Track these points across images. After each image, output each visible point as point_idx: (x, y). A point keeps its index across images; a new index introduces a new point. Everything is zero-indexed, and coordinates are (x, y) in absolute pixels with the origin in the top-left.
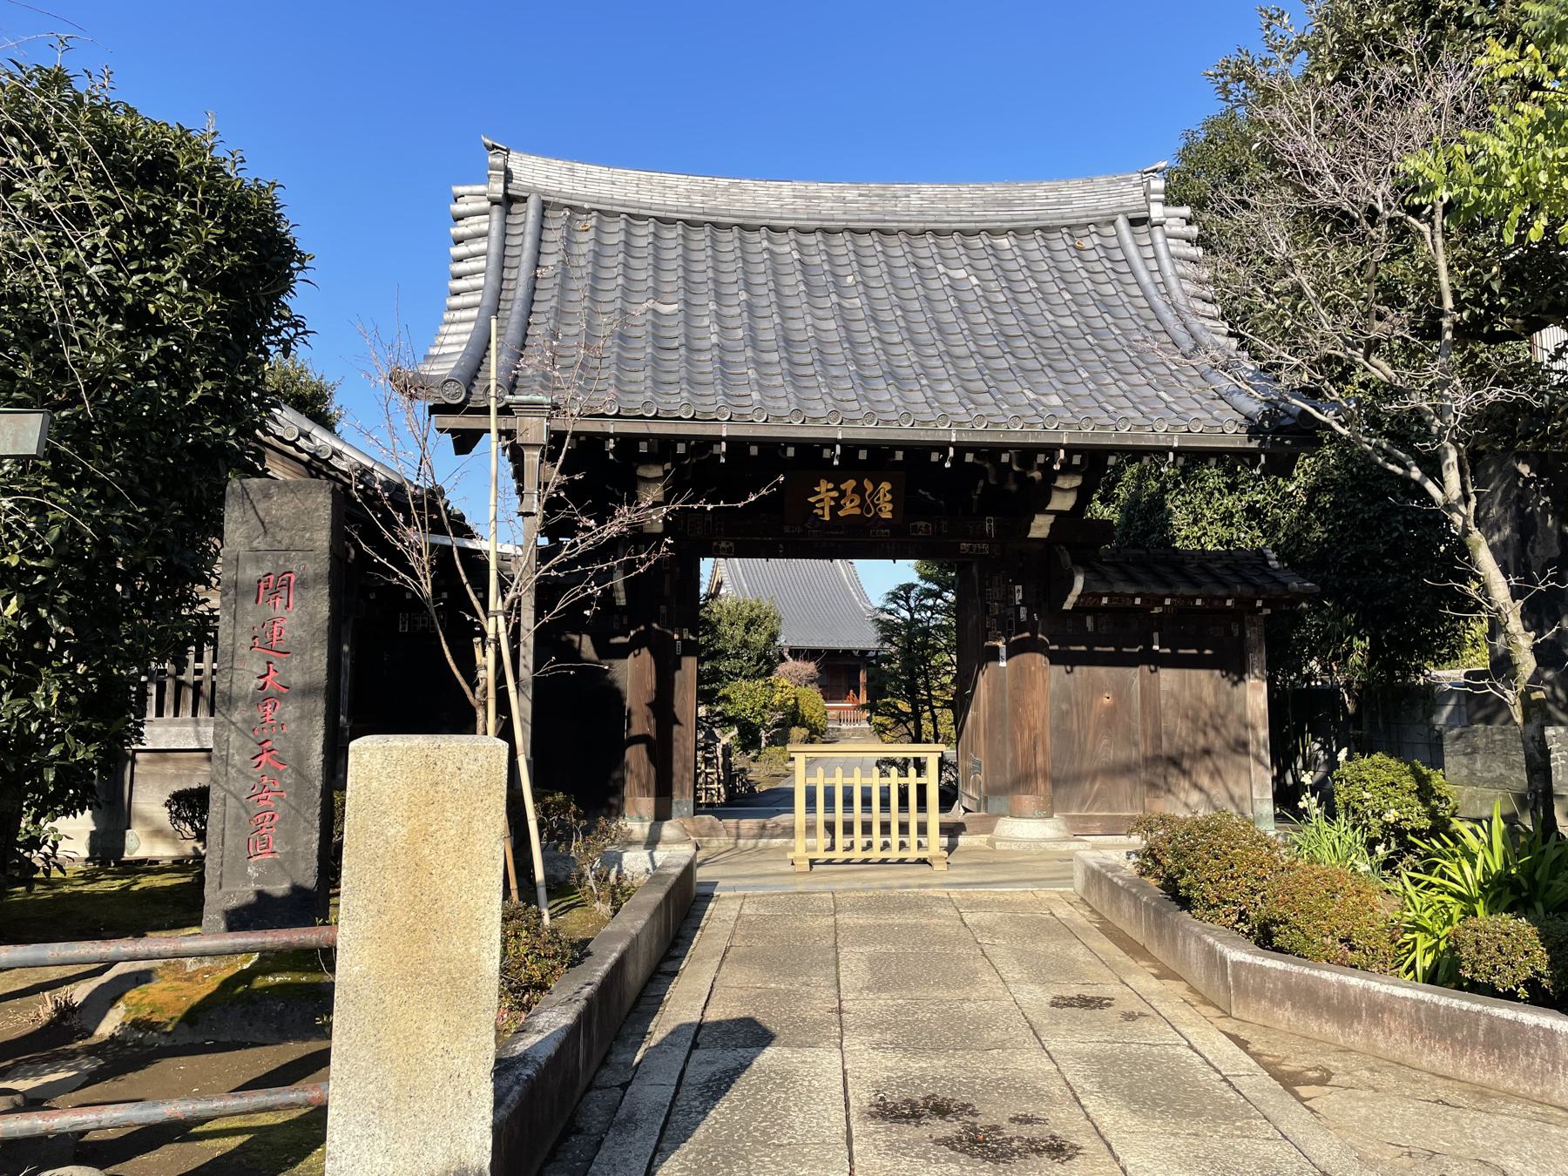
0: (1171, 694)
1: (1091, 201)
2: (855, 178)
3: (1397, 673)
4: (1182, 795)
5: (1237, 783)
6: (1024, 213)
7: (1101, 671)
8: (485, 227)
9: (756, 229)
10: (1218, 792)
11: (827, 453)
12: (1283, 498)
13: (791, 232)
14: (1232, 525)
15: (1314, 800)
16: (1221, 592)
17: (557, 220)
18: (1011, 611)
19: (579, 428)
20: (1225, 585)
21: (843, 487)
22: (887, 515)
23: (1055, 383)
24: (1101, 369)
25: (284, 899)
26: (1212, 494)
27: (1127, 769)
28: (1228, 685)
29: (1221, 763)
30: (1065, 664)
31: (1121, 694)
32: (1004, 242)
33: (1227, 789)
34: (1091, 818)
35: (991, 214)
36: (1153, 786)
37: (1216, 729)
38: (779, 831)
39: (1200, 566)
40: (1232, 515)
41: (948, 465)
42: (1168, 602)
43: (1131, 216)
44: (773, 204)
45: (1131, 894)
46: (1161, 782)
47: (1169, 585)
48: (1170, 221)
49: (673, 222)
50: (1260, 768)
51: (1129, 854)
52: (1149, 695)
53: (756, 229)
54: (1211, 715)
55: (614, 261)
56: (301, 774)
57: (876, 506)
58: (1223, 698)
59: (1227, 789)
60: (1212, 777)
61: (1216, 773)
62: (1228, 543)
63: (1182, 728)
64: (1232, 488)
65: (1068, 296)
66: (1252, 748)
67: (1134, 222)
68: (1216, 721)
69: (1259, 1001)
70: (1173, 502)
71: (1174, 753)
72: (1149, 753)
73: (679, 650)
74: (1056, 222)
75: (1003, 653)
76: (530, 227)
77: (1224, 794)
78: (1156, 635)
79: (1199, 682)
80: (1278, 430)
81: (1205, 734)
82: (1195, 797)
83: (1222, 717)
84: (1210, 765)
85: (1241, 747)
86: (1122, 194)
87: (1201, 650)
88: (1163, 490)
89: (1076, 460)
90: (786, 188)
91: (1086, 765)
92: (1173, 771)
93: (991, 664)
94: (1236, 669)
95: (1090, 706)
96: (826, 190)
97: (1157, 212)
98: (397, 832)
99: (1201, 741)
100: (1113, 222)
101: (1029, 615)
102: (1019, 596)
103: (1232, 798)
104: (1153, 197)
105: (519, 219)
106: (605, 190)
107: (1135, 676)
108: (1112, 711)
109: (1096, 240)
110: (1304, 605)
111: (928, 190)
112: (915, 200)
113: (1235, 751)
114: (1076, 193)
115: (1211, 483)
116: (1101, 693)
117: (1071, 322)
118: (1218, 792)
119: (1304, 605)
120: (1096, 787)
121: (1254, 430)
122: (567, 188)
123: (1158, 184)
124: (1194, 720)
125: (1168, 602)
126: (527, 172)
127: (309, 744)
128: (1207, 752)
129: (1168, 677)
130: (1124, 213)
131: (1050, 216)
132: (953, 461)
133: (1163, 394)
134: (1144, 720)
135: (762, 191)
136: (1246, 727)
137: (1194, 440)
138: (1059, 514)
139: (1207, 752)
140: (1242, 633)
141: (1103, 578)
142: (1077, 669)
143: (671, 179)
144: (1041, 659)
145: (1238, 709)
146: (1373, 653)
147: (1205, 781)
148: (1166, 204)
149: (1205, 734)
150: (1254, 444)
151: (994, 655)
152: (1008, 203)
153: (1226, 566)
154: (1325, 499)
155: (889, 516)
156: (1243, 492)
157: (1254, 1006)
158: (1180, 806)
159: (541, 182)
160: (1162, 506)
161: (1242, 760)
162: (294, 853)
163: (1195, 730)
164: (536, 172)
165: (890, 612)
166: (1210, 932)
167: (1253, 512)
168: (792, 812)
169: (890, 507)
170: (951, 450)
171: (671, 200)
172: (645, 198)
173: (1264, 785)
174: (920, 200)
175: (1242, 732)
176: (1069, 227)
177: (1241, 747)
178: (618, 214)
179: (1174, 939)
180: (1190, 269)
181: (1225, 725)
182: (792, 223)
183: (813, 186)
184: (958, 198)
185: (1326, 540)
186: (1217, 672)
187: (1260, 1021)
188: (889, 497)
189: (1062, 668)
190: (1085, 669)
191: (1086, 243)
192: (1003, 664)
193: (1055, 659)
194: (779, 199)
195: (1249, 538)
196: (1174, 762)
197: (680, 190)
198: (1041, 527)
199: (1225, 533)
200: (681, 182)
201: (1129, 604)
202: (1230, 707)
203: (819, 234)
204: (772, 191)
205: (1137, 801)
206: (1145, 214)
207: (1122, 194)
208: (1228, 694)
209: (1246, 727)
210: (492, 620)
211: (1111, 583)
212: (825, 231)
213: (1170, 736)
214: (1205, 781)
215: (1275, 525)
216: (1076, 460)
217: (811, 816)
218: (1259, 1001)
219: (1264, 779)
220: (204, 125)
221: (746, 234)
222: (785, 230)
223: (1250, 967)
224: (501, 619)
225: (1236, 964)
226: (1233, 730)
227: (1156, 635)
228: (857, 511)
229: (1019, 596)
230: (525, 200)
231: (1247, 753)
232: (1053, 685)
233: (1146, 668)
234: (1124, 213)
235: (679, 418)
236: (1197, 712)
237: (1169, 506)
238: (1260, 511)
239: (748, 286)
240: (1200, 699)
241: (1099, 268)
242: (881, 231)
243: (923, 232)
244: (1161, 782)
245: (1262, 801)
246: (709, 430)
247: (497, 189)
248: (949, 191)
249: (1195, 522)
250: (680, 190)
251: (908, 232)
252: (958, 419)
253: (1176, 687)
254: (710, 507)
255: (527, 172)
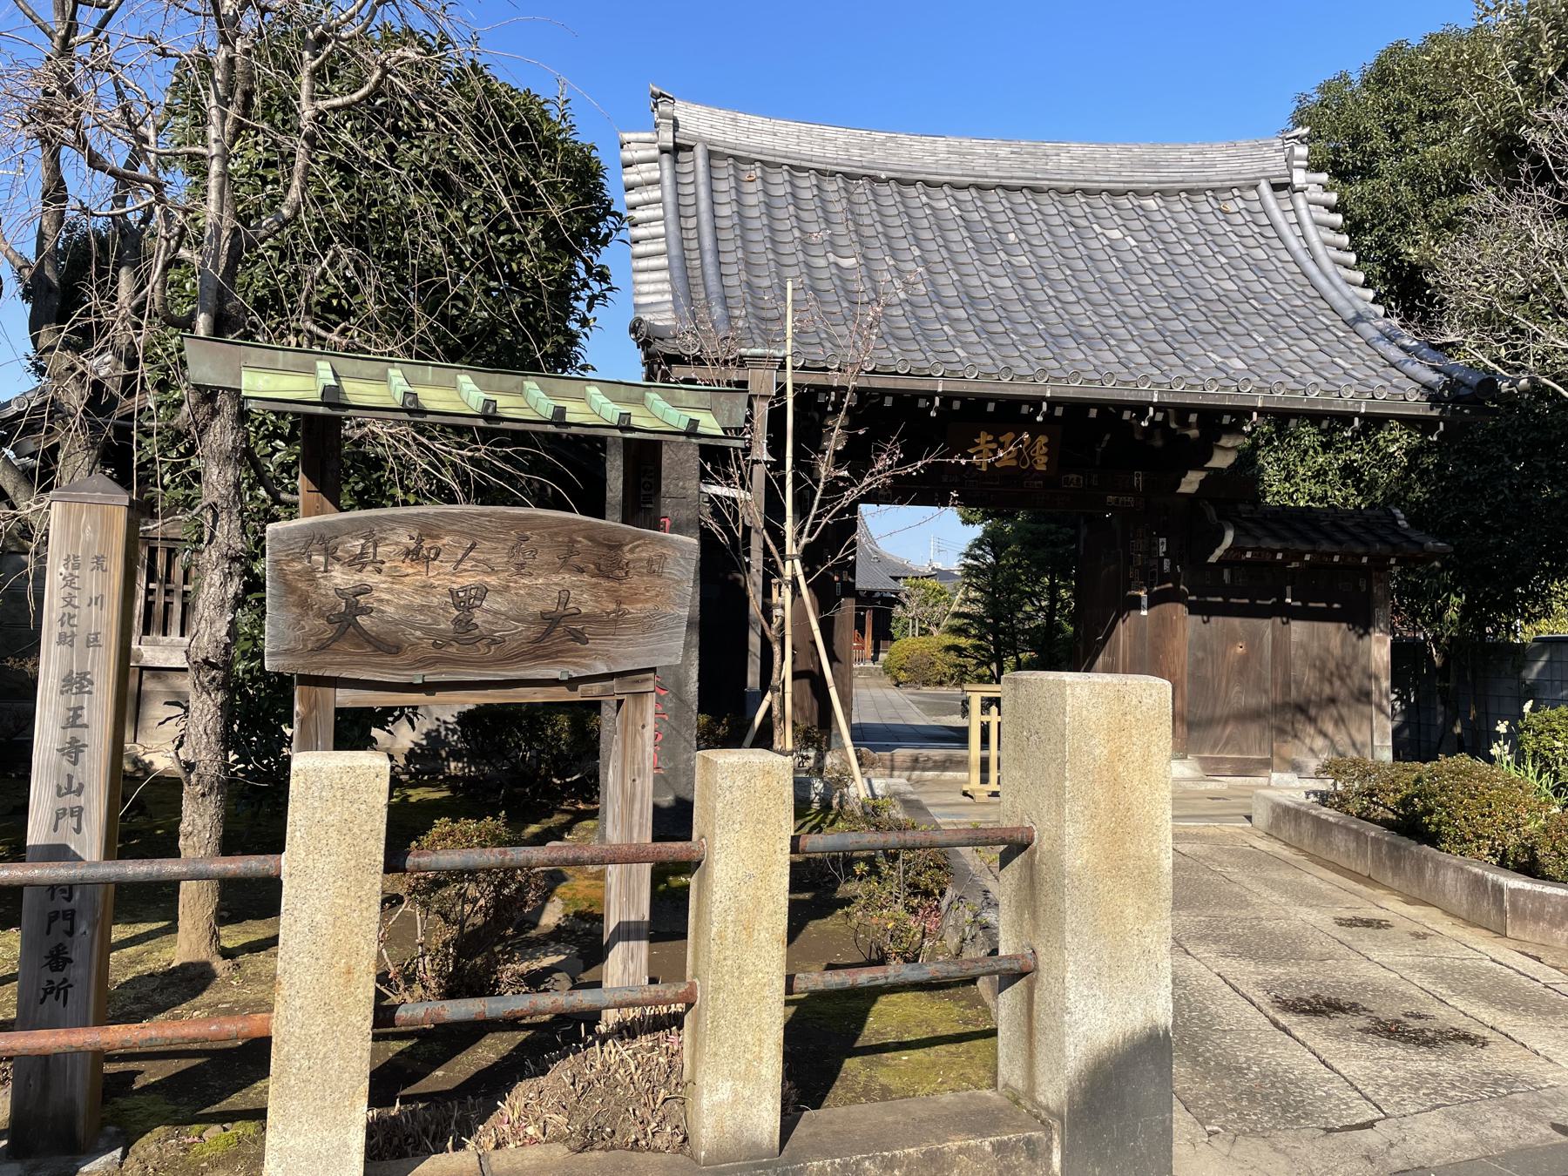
0: (1301, 645)
1: (1234, 164)
2: (1007, 139)
3: (1489, 630)
4: (1308, 741)
5: (1359, 730)
6: (1169, 175)
7: (1236, 622)
8: (656, 175)
9: (913, 183)
10: (1341, 739)
11: (821, 399)
12: (1382, 459)
13: (919, 185)
14: (1324, 482)
15: (1507, 748)
16: (1360, 550)
17: (725, 169)
18: (1155, 562)
19: (864, 383)
20: (1365, 543)
21: (1001, 439)
22: (1041, 467)
23: (1235, 347)
24: (1272, 333)
25: (670, 809)
26: (1306, 452)
27: (1256, 715)
28: (1354, 639)
29: (1345, 711)
30: (1281, 616)
31: (1253, 642)
32: (1150, 203)
33: (1350, 736)
34: (1222, 760)
35: (1138, 176)
36: (1281, 731)
37: (1342, 679)
38: (930, 764)
39: (1333, 524)
40: (1326, 473)
41: (1039, 419)
42: (1307, 558)
43: (1274, 181)
44: (929, 160)
45: (1349, 830)
46: (1289, 728)
47: (1313, 542)
48: (1311, 187)
49: (833, 174)
50: (1382, 717)
51: (1308, 794)
52: (1279, 646)
53: (913, 183)
54: (1337, 665)
55: (785, 212)
56: (681, 701)
57: (1031, 458)
58: (1350, 650)
59: (1350, 736)
60: (1336, 724)
61: (1340, 721)
62: (1323, 498)
63: (1309, 677)
64: (1326, 447)
65: (1223, 260)
66: (1375, 697)
67: (1276, 187)
68: (1342, 671)
69: (1537, 923)
70: (1266, 458)
71: (1301, 700)
72: (1279, 700)
73: (839, 592)
74: (1202, 185)
75: (1145, 602)
76: (702, 177)
77: (1348, 741)
78: (1289, 589)
79: (1327, 634)
80: (1456, 400)
81: (1331, 683)
82: (1319, 743)
83: (1348, 668)
84: (1335, 713)
85: (1364, 696)
86: (1264, 159)
87: (1330, 604)
88: (1255, 447)
89: (1059, 412)
90: (941, 144)
91: (1218, 712)
92: (1299, 717)
93: (1133, 613)
94: (1361, 622)
95: (1224, 655)
96: (979, 147)
97: (1299, 177)
98: (1101, 752)
99: (1327, 690)
100: (1256, 187)
101: (1172, 567)
102: (1163, 549)
103: (1354, 744)
104: (1296, 163)
105: (688, 168)
106: (767, 141)
107: (1267, 627)
108: (1245, 659)
109: (1241, 204)
110: (1437, 564)
111: (1077, 149)
112: (1065, 159)
113: (1358, 700)
114: (1219, 156)
115: (1306, 441)
116: (1235, 642)
117: (1230, 285)
118: (1341, 739)
119: (1437, 564)
120: (1228, 731)
121: (1434, 398)
122: (730, 139)
123: (1302, 151)
124: (1322, 671)
125: (1307, 558)
126: (692, 121)
127: (687, 672)
128: (1332, 700)
129: (1298, 629)
130: (1267, 178)
131: (1195, 179)
132: (1045, 416)
133: (1338, 360)
134: (1274, 668)
135: (918, 146)
136: (1370, 677)
137: (1381, 406)
138: (1199, 467)
139: (1332, 700)
140: (1370, 588)
141: (1248, 533)
142: (1213, 619)
143: (830, 132)
144: (1181, 609)
145: (1362, 661)
146: (1465, 611)
147: (1329, 728)
148: (1307, 169)
149: (1331, 683)
150: (1435, 413)
151: (1136, 604)
152: (1154, 165)
153: (1358, 525)
154: (1429, 461)
155: (1044, 468)
156: (1340, 451)
157: (1531, 927)
158: (1305, 750)
159: (706, 131)
160: (1254, 462)
161: (1366, 709)
162: (675, 769)
163: (1322, 679)
164: (700, 121)
165: (975, 558)
166: (1470, 863)
167: (1348, 470)
168: (966, 748)
169: (1045, 459)
170: (1045, 405)
171: (830, 152)
172: (805, 150)
173: (1384, 733)
174: (1069, 159)
175: (1366, 682)
176: (1213, 190)
177: (1364, 696)
178: (780, 166)
179: (1420, 871)
180: (1330, 236)
181: (1349, 676)
182: (947, 178)
183: (966, 142)
184: (1107, 158)
185: (1426, 501)
186: (1344, 625)
187: (1538, 940)
188: (1045, 449)
189: (1199, 618)
190: (1221, 619)
191: (1231, 207)
192: (1144, 613)
193: (1194, 609)
194: (934, 154)
195: (1341, 495)
196: (1301, 709)
197: (839, 142)
198: (1191, 482)
199: (1318, 490)
200: (839, 135)
201: (1268, 557)
202: (1355, 658)
203: (973, 190)
204: (928, 146)
205: (1265, 746)
206: (1287, 180)
207: (1264, 159)
208: (1354, 646)
209: (1370, 677)
210: (788, 563)
211: (1258, 539)
212: (979, 187)
213: (1299, 684)
214: (1329, 728)
215: (1373, 483)
216: (1059, 412)
217: (985, 753)
218: (1537, 923)
219: (1385, 727)
220: (543, 92)
221: (904, 189)
222: (940, 185)
223: (1527, 894)
224: (797, 562)
225: (1514, 892)
226: (1357, 680)
227: (1289, 589)
228: (1014, 463)
229: (1163, 549)
230: (691, 148)
231: (1370, 703)
232: (1189, 632)
233: (1278, 620)
234: (1267, 178)
235: (896, 373)
236: (1323, 662)
237: (1261, 461)
238: (1357, 470)
239: (918, 242)
240: (1327, 650)
241: (1247, 232)
242: (1032, 189)
243: (1073, 191)
244: (1289, 728)
245: (1382, 747)
246: (925, 385)
247: (667, 138)
248: (1098, 151)
249: (1287, 479)
250: (839, 142)
251: (1059, 191)
252: (985, 370)
253: (1305, 639)
254: (963, 462)
255: (692, 121)
